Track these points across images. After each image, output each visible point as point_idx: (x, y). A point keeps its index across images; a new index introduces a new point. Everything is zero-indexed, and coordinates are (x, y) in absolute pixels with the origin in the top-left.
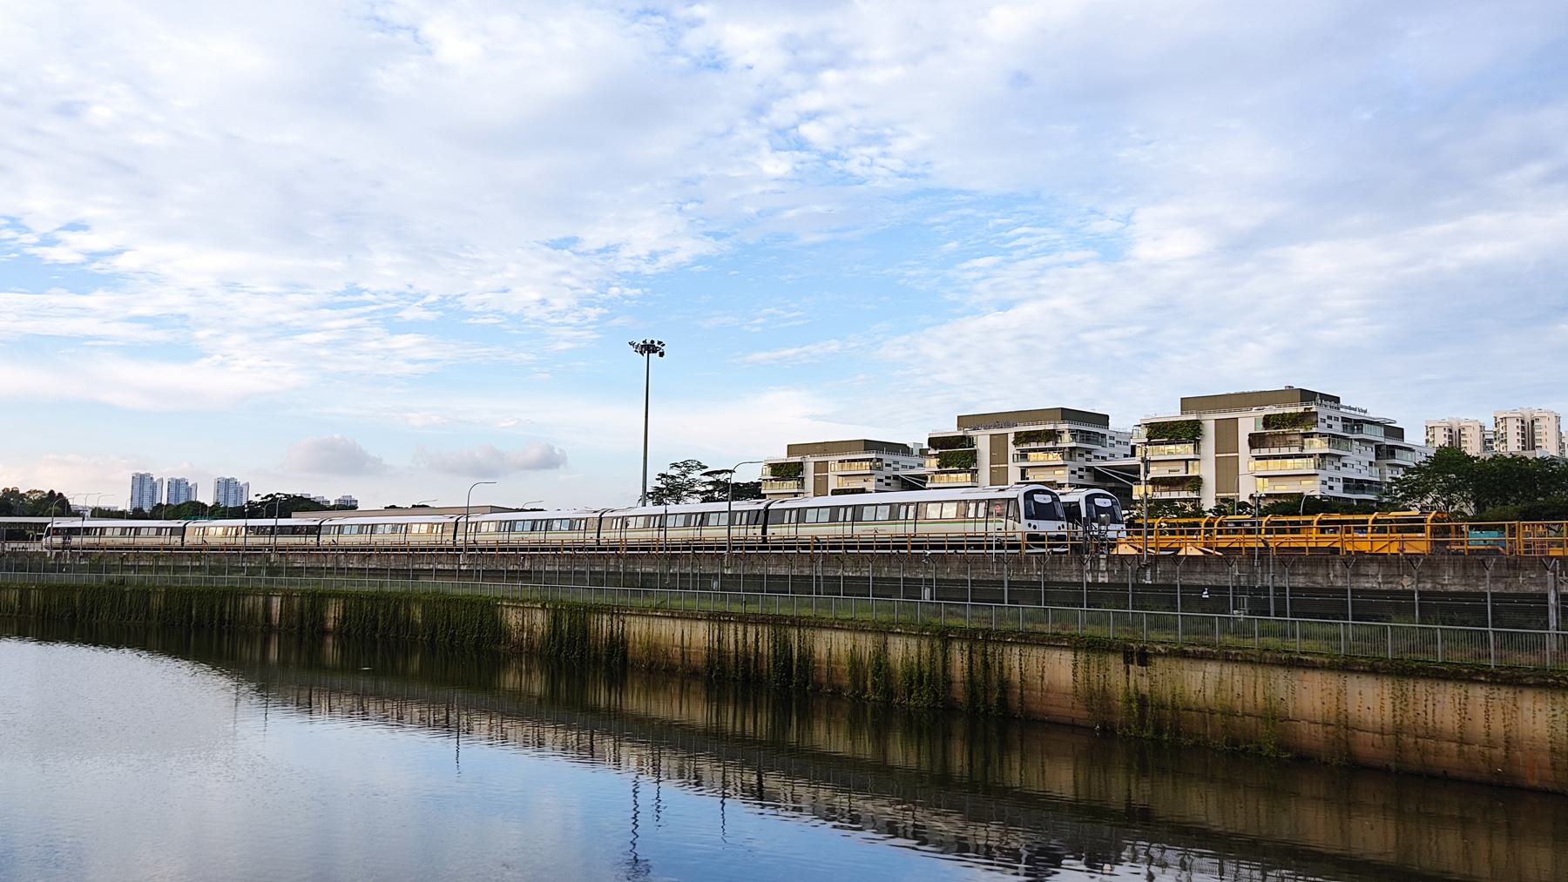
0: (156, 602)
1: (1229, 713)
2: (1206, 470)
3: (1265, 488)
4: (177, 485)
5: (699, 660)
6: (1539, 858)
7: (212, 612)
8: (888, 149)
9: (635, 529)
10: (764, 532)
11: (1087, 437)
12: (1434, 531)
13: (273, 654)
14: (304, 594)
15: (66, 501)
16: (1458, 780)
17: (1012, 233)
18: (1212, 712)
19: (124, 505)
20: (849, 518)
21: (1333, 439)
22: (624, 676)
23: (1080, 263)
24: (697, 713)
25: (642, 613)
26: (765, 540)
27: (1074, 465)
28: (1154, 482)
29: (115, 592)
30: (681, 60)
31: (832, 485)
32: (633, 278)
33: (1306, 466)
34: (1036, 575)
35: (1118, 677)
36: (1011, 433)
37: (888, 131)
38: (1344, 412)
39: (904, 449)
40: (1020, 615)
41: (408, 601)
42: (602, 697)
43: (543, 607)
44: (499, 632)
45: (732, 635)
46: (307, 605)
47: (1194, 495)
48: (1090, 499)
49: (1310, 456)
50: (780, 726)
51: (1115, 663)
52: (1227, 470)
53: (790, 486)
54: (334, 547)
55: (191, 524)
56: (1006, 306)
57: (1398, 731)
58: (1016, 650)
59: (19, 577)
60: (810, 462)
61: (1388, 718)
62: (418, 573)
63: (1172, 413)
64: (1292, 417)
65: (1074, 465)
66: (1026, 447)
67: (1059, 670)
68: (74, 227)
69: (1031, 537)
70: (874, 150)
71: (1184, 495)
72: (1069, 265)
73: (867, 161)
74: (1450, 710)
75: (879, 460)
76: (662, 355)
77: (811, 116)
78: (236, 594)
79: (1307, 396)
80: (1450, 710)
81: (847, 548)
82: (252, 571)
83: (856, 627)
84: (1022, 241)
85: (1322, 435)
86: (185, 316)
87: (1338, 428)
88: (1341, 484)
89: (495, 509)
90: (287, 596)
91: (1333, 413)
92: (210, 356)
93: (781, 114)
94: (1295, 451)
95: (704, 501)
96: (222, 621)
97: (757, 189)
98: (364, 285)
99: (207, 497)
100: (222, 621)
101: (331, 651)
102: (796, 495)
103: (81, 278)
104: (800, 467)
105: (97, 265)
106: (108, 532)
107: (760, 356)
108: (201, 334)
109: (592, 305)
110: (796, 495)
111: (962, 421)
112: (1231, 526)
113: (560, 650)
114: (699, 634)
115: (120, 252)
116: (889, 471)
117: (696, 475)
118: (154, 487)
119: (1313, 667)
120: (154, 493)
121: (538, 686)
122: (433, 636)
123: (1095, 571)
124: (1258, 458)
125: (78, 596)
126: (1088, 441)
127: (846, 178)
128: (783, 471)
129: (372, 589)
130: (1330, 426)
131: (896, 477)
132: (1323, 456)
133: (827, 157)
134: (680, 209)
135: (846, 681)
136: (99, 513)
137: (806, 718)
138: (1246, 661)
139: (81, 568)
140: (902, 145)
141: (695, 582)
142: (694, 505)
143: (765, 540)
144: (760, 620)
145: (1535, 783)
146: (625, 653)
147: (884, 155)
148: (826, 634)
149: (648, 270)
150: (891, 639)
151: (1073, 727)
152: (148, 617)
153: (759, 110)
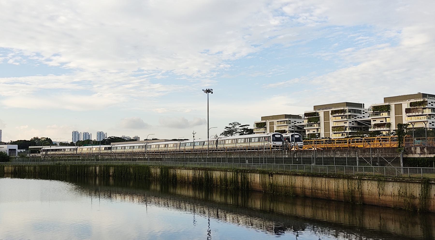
0: (68, 169)
1: (286, 187)
4: (86, 134)
5: (191, 180)
7: (82, 172)
9: (228, 144)
11: (355, 111)
13: (97, 182)
14: (104, 166)
16: (321, 199)
17: (356, 39)
19: (70, 141)
22: (176, 184)
23: (383, 48)
24: (191, 193)
27: (350, 120)
28: (375, 125)
29: (58, 167)
33: (424, 119)
34: (273, 156)
35: (268, 179)
36: (330, 110)
39: (298, 117)
41: (129, 167)
42: (171, 190)
44: (150, 174)
45: (197, 173)
46: (105, 169)
48: (292, 136)
49: (425, 115)
50: (207, 195)
51: (267, 176)
53: (262, 130)
54: (115, 153)
59: (34, 163)
62: (135, 160)
63: (381, 102)
65: (350, 120)
66: (335, 115)
68: (55, 55)
69: (274, 146)
70: (307, 15)
71: (385, 129)
73: (305, 18)
74: (322, 184)
75: (290, 121)
76: (212, 93)
78: (88, 166)
79: (424, 95)
80: (322, 184)
83: (221, 170)
84: (359, 42)
86: (90, 81)
90: (100, 167)
94: (420, 113)
95: (240, 135)
96: (84, 173)
98: (143, 68)
99: (94, 138)
100: (84, 173)
101: (111, 181)
102: (264, 132)
103: (60, 70)
104: (265, 124)
105: (64, 66)
108: (95, 86)
114: (191, 173)
115: (70, 62)
116: (353, 119)
117: (237, 127)
118: (79, 135)
120: (79, 137)
121: (158, 188)
122: (135, 176)
123: (285, 154)
124: (409, 116)
125: (48, 168)
126: (355, 112)
128: (260, 125)
129: (121, 164)
133: (292, 17)
135: (219, 183)
136: (62, 144)
137: (212, 193)
139: (50, 160)
140: (318, 12)
141: (265, 161)
142: (237, 136)
144: (199, 169)
145: (333, 199)
146: (176, 179)
147: (311, 16)
148: (215, 172)
150: (228, 173)
151: (260, 192)
152: (66, 173)
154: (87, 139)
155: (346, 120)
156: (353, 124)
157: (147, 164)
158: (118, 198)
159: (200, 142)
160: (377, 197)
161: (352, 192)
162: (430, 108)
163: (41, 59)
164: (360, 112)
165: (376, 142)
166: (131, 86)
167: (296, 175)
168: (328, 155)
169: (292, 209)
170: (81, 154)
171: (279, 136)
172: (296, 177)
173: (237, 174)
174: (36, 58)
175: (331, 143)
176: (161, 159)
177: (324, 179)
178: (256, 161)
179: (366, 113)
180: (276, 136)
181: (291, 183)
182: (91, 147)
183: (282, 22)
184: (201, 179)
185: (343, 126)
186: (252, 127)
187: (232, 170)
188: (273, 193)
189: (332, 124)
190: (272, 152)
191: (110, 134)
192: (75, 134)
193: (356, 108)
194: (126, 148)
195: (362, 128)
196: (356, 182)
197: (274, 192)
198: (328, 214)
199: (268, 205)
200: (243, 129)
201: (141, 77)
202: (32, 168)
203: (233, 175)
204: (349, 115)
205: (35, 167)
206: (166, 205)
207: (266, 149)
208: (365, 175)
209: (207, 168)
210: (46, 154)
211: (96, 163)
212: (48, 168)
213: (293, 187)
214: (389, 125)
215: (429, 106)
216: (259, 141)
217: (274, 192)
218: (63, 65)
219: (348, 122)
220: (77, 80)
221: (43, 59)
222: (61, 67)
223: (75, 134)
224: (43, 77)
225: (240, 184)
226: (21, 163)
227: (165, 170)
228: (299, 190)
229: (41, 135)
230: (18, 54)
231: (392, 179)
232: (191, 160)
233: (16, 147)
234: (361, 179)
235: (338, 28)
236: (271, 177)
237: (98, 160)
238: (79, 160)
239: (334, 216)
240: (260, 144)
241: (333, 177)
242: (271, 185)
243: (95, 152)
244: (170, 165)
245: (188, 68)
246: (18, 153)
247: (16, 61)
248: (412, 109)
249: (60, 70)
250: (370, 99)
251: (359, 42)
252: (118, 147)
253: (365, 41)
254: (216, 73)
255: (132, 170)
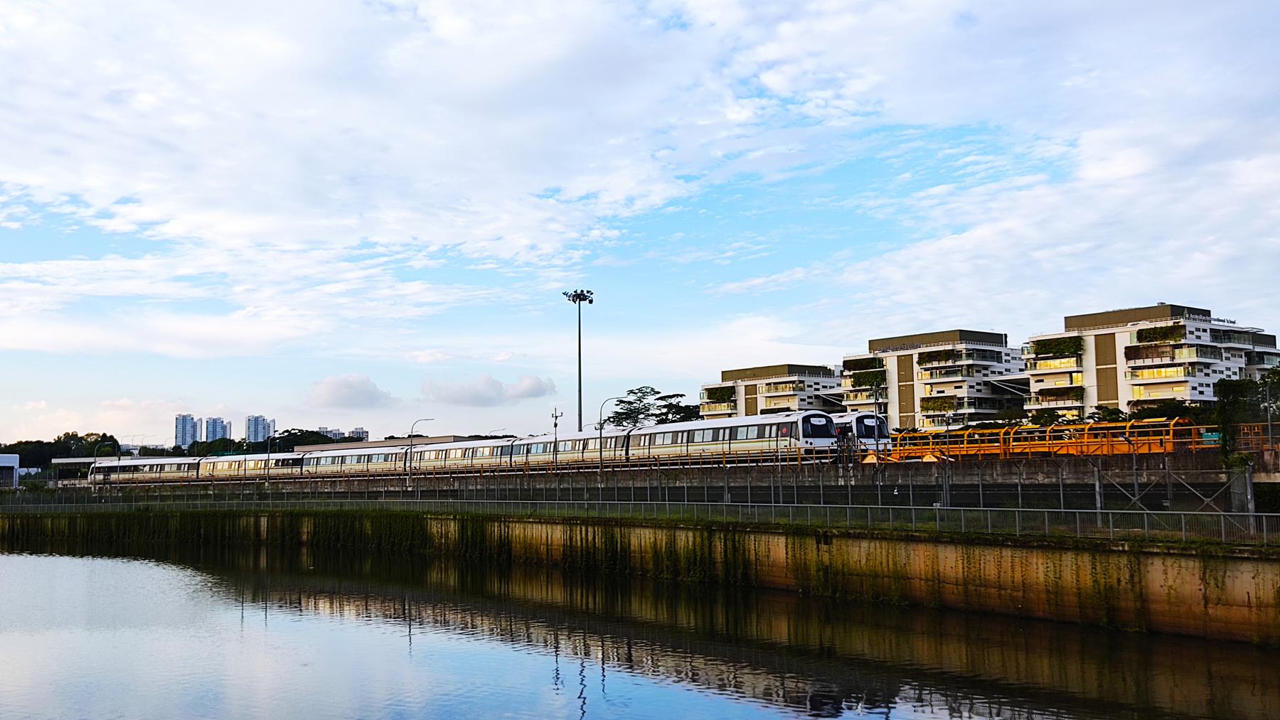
0: (174, 524)
1: (876, 576)
2: (1088, 380)
3: (1143, 395)
4: (214, 424)
5: (557, 555)
6: (1249, 701)
8: (842, 91)
10: (627, 453)
11: (983, 355)
12: (1176, 434)
13: (263, 563)
14: (284, 514)
15: (116, 441)
17: (960, 162)
18: (865, 575)
19: (170, 444)
20: (727, 437)
21: (1202, 350)
23: (1029, 187)
24: (557, 595)
25: (520, 520)
26: (628, 459)
28: (1042, 393)
30: (649, 22)
31: (762, 405)
32: (610, 221)
33: (1176, 374)
35: (812, 552)
36: (915, 353)
37: (841, 75)
38: (1216, 325)
39: (824, 371)
40: (753, 511)
42: (495, 587)
43: (455, 518)
44: (426, 538)
45: (579, 534)
46: (286, 523)
47: (1078, 404)
49: (1180, 365)
51: (811, 543)
52: (1107, 381)
53: (723, 408)
55: (204, 461)
56: (960, 229)
57: (966, 583)
58: (752, 537)
60: (741, 386)
61: (960, 575)
63: (1057, 330)
64: (1163, 330)
66: (929, 366)
67: (778, 549)
68: (125, 201)
69: (808, 451)
70: (828, 94)
71: (1069, 403)
72: (1020, 188)
73: (823, 103)
74: (997, 565)
76: (591, 302)
77: (770, 65)
78: (234, 516)
79: (1177, 311)
80: (997, 565)
81: (683, 464)
82: (250, 497)
83: (655, 525)
84: (970, 169)
85: (1191, 346)
86: (225, 274)
87: (1206, 339)
88: (1211, 389)
89: (457, 439)
90: (272, 517)
91: (1203, 325)
92: (244, 308)
93: (743, 64)
94: (1167, 361)
95: (660, 422)
97: (724, 134)
98: (374, 239)
101: (305, 559)
102: (730, 415)
103: (137, 243)
104: (732, 390)
106: (167, 468)
107: (731, 286)
108: (238, 289)
109: (575, 248)
110: (730, 415)
111: (873, 345)
112: (977, 437)
113: (466, 551)
114: (557, 534)
117: (650, 399)
118: (194, 426)
119: (918, 540)
121: (453, 580)
125: (113, 521)
126: (984, 358)
127: (804, 120)
128: (719, 395)
129: (335, 509)
130: (1199, 337)
131: (817, 397)
132: (1190, 364)
133: (785, 101)
134: (653, 156)
135: (651, 565)
136: (146, 452)
138: (884, 539)
139: (117, 499)
140: (855, 87)
143: (628, 459)
145: (1041, 614)
147: (838, 97)
148: (638, 531)
149: (625, 213)
150: (678, 533)
151: (787, 591)
153: (722, 63)
154: (219, 436)
155: (960, 378)
156: (979, 391)
157: (418, 508)
158: (346, 613)
159: (545, 444)
160: (1198, 609)
161: (1107, 595)
162: (1192, 346)
163: (83, 212)
164: (997, 357)
165: (1086, 440)
166: (340, 287)
167: (910, 539)
168: (987, 478)
169: (898, 645)
170: (211, 478)
171: (823, 421)
172: (911, 547)
173: (710, 538)
174: (68, 209)
175: (956, 443)
176: (454, 494)
177: (1007, 553)
178: (761, 495)
179: (1014, 358)
180: (814, 421)
181: (895, 564)
182: (241, 457)
183: (760, 112)
184: (589, 552)
185: (952, 397)
186: (692, 398)
187: (691, 525)
188: (833, 597)
189: (921, 391)
190: (802, 470)
191: (283, 425)
192: (184, 422)
193: (987, 344)
194: (323, 461)
195: (1006, 399)
196: (1124, 560)
197: (834, 592)
198: (1022, 663)
199: (815, 634)
200: (665, 406)
201: (369, 262)
202: (64, 523)
203: (698, 539)
204: (969, 366)
205: (72, 520)
206: (468, 628)
207: (784, 460)
208: (1153, 540)
209: (610, 520)
210: (105, 482)
211: (257, 505)
212: (113, 521)
213: (902, 577)
214: (1079, 393)
215: (1191, 339)
216: (715, 439)
217: (834, 592)
218: (146, 229)
219: (965, 386)
220: (181, 272)
221: (91, 212)
222: (139, 235)
223: (184, 422)
224: (88, 263)
225: (720, 567)
226: (31, 508)
227: (474, 527)
228: (920, 587)
229: (84, 426)
230: (19, 197)
231: (1253, 553)
232: (550, 494)
233: (13, 460)
234: (1140, 552)
235: (912, 131)
236: (824, 547)
237: (263, 496)
238: (207, 496)
239: (1044, 670)
240: (764, 445)
241: (1038, 547)
242: (825, 569)
243: (254, 472)
244: (488, 511)
245: (500, 239)
246: (21, 477)
247: (11, 217)
248: (1144, 347)
249: (137, 243)
250: (1025, 321)
251: (970, 169)
252: (323, 460)
253: (984, 166)
254: (581, 252)
255: (368, 525)
